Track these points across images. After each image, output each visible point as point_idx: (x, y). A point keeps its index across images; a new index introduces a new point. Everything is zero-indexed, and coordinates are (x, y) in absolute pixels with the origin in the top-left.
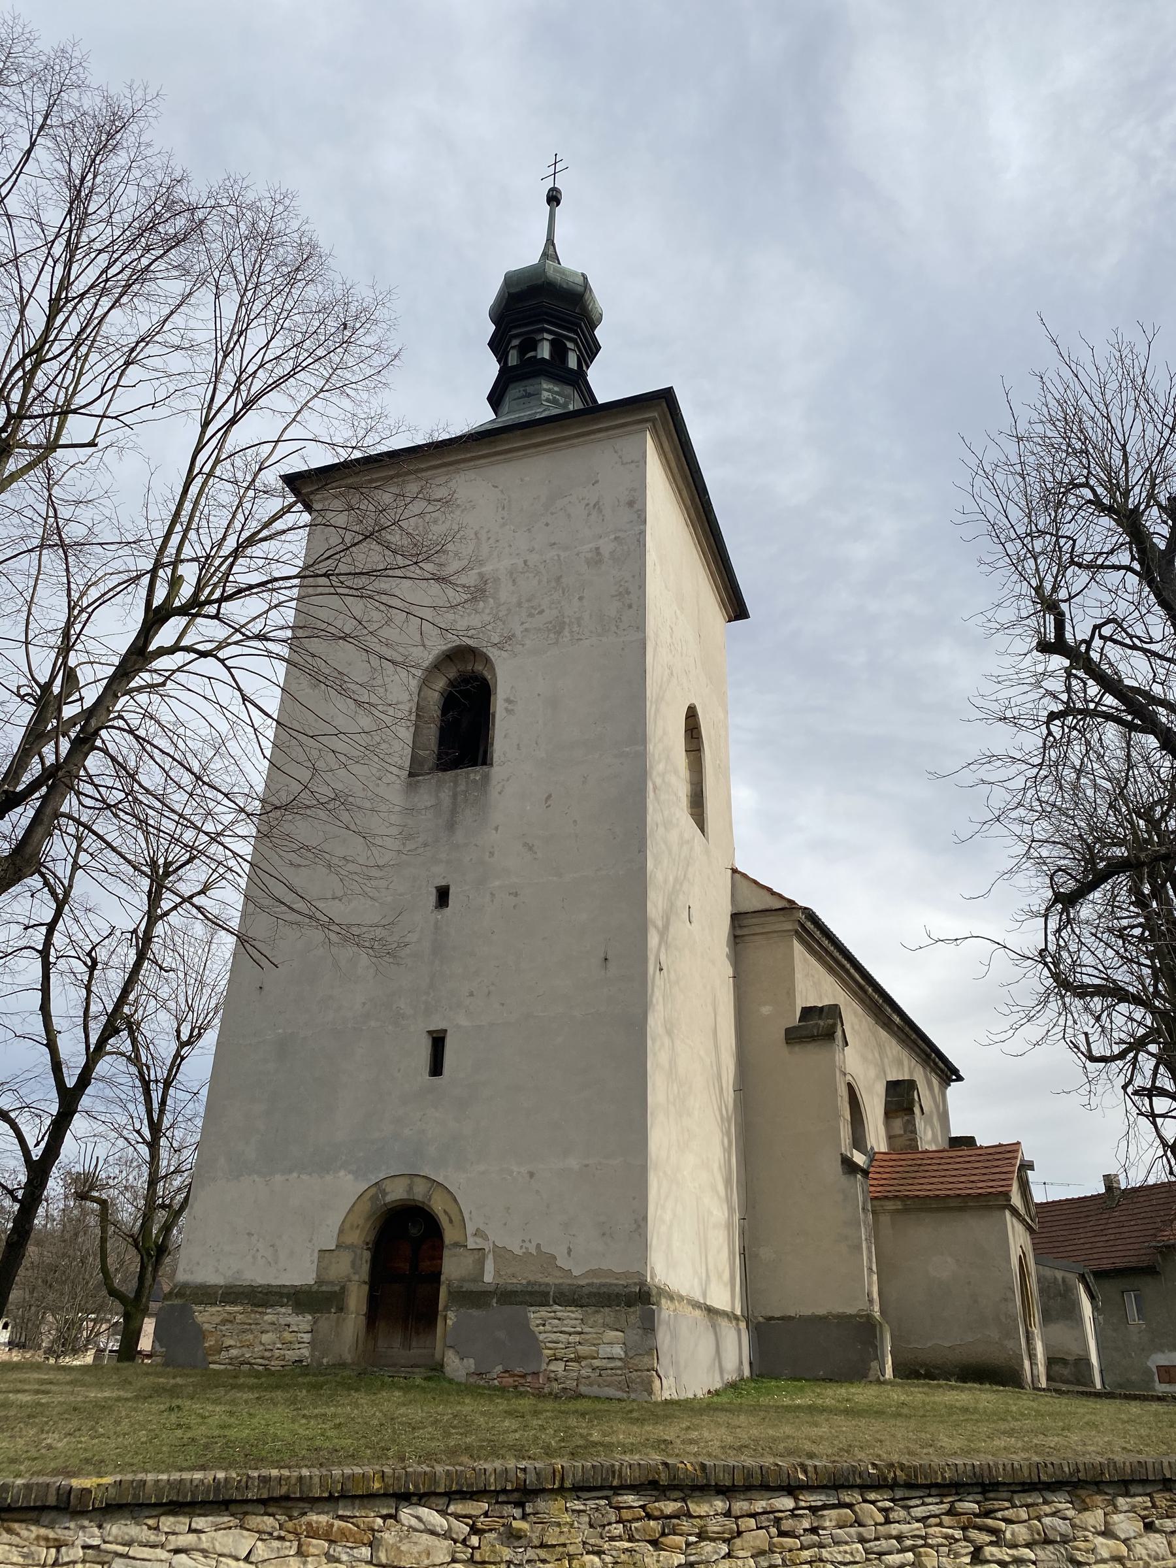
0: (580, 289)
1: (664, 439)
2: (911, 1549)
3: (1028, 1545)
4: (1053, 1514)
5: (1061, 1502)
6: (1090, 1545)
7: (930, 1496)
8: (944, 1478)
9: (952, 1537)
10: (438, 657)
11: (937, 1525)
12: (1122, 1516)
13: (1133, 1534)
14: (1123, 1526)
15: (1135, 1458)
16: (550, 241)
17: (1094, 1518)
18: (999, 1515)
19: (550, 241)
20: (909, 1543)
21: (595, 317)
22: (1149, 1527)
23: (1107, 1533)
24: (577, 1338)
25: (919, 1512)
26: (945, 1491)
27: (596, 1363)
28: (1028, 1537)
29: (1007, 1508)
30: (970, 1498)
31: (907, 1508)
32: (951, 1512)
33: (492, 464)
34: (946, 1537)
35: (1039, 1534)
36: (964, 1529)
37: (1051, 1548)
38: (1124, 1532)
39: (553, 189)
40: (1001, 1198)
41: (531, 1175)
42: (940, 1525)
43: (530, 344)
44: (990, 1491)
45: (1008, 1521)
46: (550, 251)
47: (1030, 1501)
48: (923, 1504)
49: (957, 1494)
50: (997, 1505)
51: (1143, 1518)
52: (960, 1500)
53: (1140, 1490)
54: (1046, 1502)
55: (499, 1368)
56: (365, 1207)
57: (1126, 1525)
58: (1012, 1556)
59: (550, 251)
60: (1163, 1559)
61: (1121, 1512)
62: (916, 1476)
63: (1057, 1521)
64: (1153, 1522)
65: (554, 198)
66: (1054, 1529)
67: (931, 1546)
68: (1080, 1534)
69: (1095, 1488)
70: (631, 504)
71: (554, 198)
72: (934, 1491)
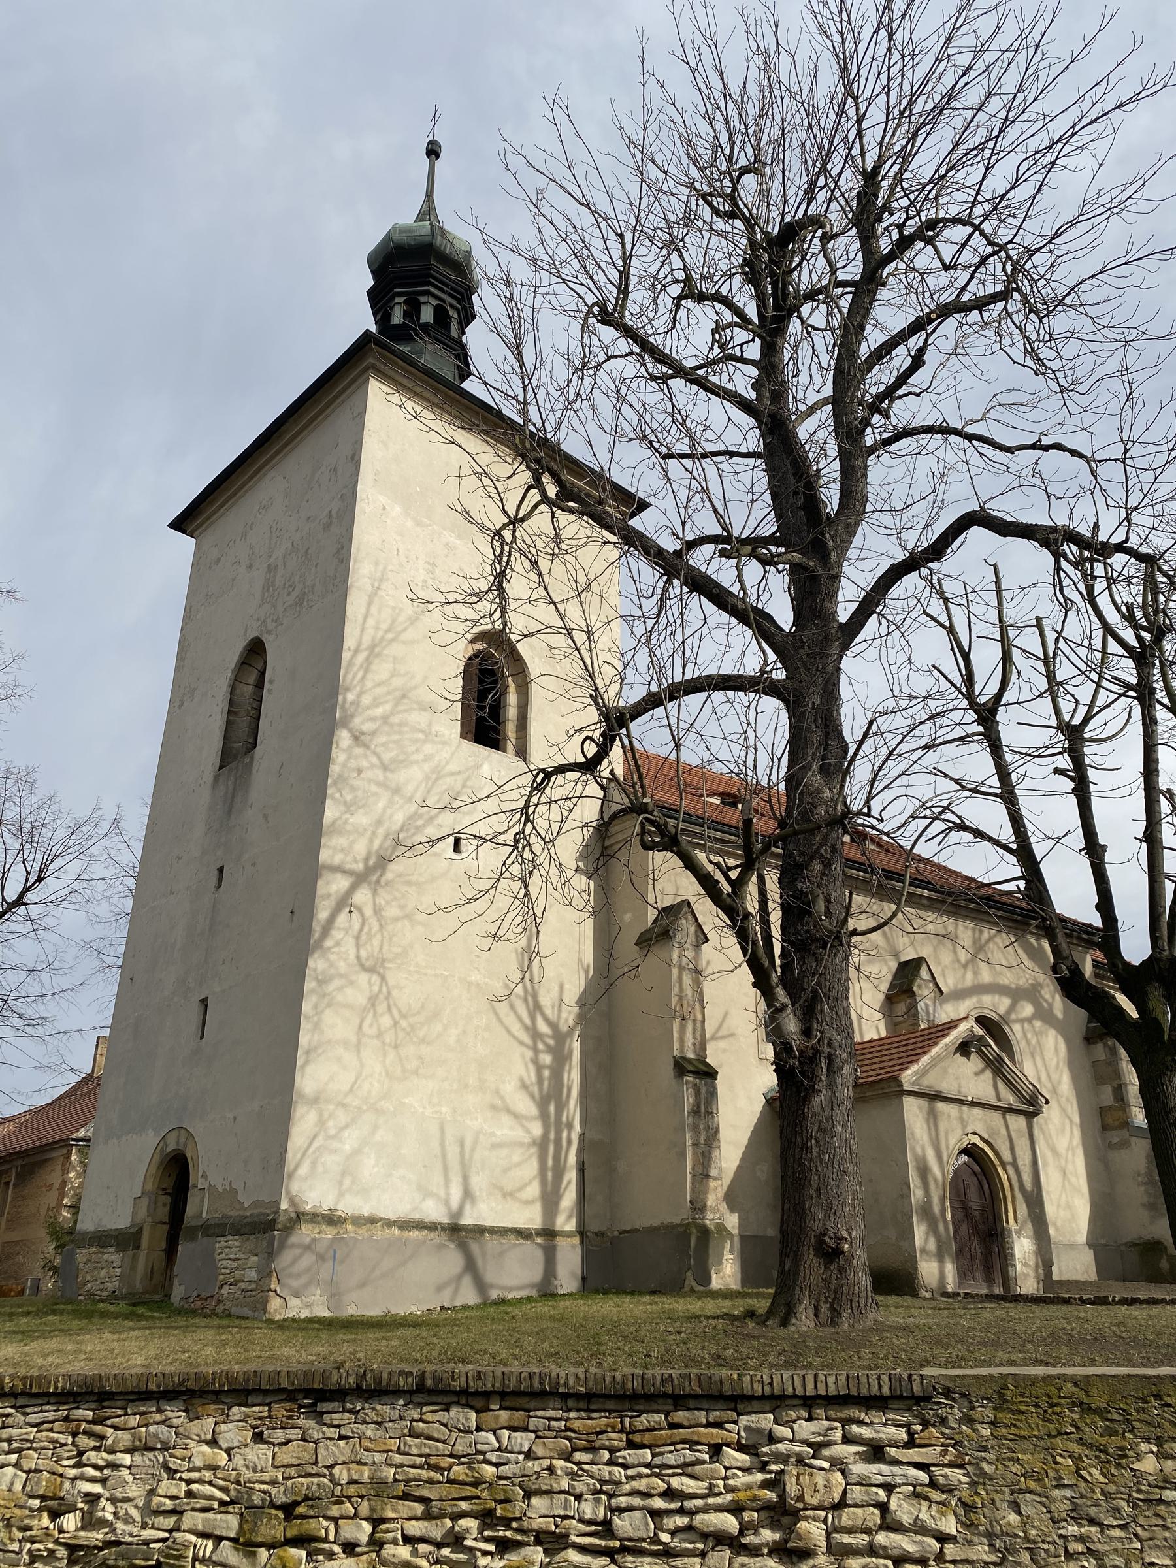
0: (428, 239)
1: (398, 378)
2: (19, 1451)
3: (130, 1451)
4: (163, 1422)
5: (176, 1415)
6: (188, 1453)
7: (48, 1403)
8: (56, 1388)
9: (57, 1441)
10: (241, 655)
11: (47, 1431)
12: (231, 1426)
13: (236, 1444)
14: (227, 1435)
15: (251, 1367)
16: (429, 197)
17: (206, 1426)
18: (109, 1422)
19: (429, 197)
20: (15, 1445)
21: (460, 258)
22: (258, 1438)
23: (213, 1442)
24: (234, 1264)
25: (33, 1419)
26: (63, 1399)
27: (243, 1286)
28: (128, 1443)
29: (120, 1416)
30: (85, 1406)
31: (25, 1414)
32: (66, 1419)
33: (285, 456)
34: (52, 1441)
35: (140, 1441)
36: (74, 1435)
37: (151, 1455)
38: (227, 1441)
39: (431, 143)
40: (893, 1084)
41: (235, 1118)
42: (51, 1430)
43: (413, 308)
44: (105, 1400)
45: (116, 1428)
46: (428, 209)
47: (143, 1409)
48: (42, 1411)
49: (74, 1402)
50: (109, 1412)
51: (254, 1427)
52: (77, 1408)
53: (259, 1400)
54: (159, 1411)
55: (195, 1294)
56: (157, 1158)
57: (231, 1434)
58: (106, 1460)
59: (428, 209)
60: (262, 1471)
61: (232, 1422)
62: (31, 1385)
63: (163, 1429)
64: (262, 1433)
65: (433, 151)
66: (156, 1436)
67: (35, 1450)
68: (179, 1441)
69: (214, 1397)
70: (353, 458)
71: (433, 151)
72: (52, 1400)
